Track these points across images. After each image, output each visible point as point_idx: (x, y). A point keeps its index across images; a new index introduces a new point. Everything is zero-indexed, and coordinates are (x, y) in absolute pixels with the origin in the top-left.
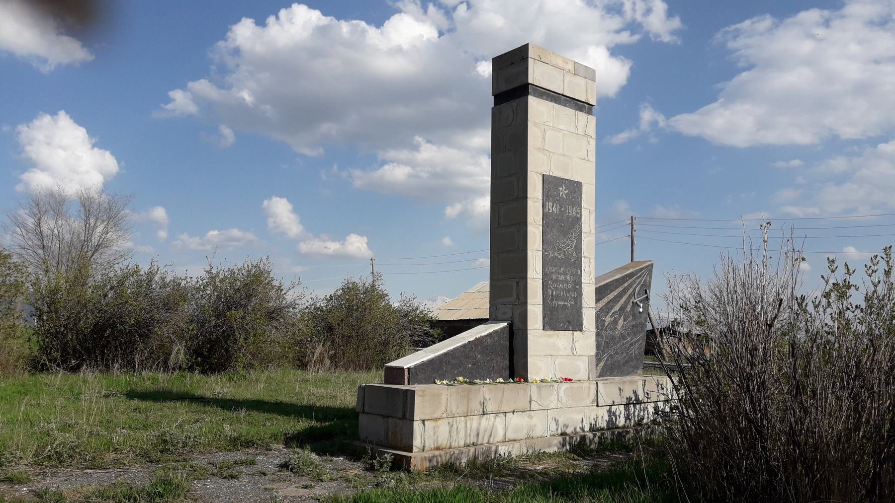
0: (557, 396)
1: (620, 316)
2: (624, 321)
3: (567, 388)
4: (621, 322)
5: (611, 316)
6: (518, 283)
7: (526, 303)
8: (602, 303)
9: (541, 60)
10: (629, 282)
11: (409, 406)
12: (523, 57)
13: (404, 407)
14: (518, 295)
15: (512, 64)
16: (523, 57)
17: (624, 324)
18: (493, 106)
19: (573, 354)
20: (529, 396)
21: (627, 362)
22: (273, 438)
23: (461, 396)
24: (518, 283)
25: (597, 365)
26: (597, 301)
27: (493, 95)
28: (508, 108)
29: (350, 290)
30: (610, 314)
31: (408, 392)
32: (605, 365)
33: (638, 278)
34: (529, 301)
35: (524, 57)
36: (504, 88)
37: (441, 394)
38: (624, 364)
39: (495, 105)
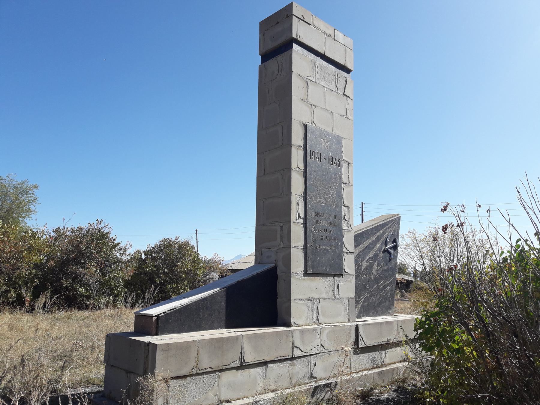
0: (320, 340)
1: (374, 262)
2: (378, 265)
3: (329, 332)
4: (375, 267)
5: (367, 262)
6: (282, 227)
7: (289, 247)
8: (361, 247)
9: (304, 20)
10: (381, 231)
11: (150, 362)
12: (287, 15)
13: (145, 363)
14: (282, 239)
15: (278, 23)
16: (287, 15)
17: (377, 269)
18: (259, 63)
19: (335, 297)
20: (292, 342)
21: (380, 303)
22: (414, 233)
23: (215, 348)
24: (282, 227)
25: (356, 306)
26: (356, 247)
27: (260, 55)
28: (272, 63)
29: (166, 245)
30: (366, 259)
31: (150, 346)
32: (363, 306)
33: (388, 228)
34: (293, 245)
35: (288, 15)
36: (271, 45)
37: (190, 346)
38: (379, 306)
39: (262, 63)
